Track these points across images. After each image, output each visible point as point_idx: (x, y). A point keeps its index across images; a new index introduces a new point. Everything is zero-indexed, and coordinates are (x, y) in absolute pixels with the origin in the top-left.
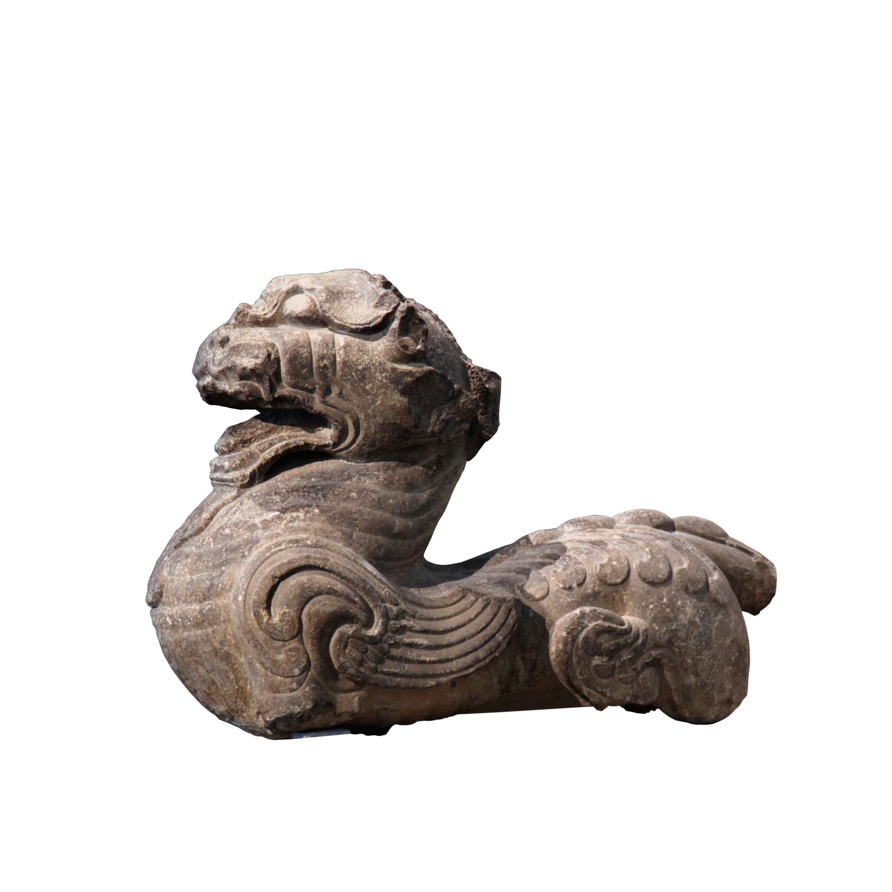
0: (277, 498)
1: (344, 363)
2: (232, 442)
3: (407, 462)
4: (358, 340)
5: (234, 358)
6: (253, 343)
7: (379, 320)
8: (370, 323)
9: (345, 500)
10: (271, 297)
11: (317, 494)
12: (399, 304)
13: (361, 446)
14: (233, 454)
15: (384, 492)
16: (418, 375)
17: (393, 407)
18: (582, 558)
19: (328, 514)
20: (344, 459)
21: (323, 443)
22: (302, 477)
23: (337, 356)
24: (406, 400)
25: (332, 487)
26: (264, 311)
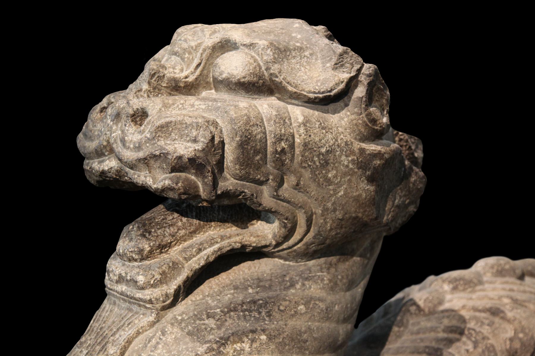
0: (211, 323)
1: (305, 145)
2: (147, 248)
3: (347, 254)
4: (316, 113)
5: (162, 143)
6: (188, 121)
7: (342, 86)
8: (330, 91)
9: (293, 316)
10: (190, 53)
11: (260, 313)
12: (363, 65)
13: (307, 245)
14: (147, 262)
15: (330, 298)
16: (386, 156)
17: (357, 199)
18: (486, 330)
19: (277, 340)
20: (280, 257)
21: (263, 243)
22: (236, 288)
23: (296, 136)
24: (372, 188)
25: (275, 300)
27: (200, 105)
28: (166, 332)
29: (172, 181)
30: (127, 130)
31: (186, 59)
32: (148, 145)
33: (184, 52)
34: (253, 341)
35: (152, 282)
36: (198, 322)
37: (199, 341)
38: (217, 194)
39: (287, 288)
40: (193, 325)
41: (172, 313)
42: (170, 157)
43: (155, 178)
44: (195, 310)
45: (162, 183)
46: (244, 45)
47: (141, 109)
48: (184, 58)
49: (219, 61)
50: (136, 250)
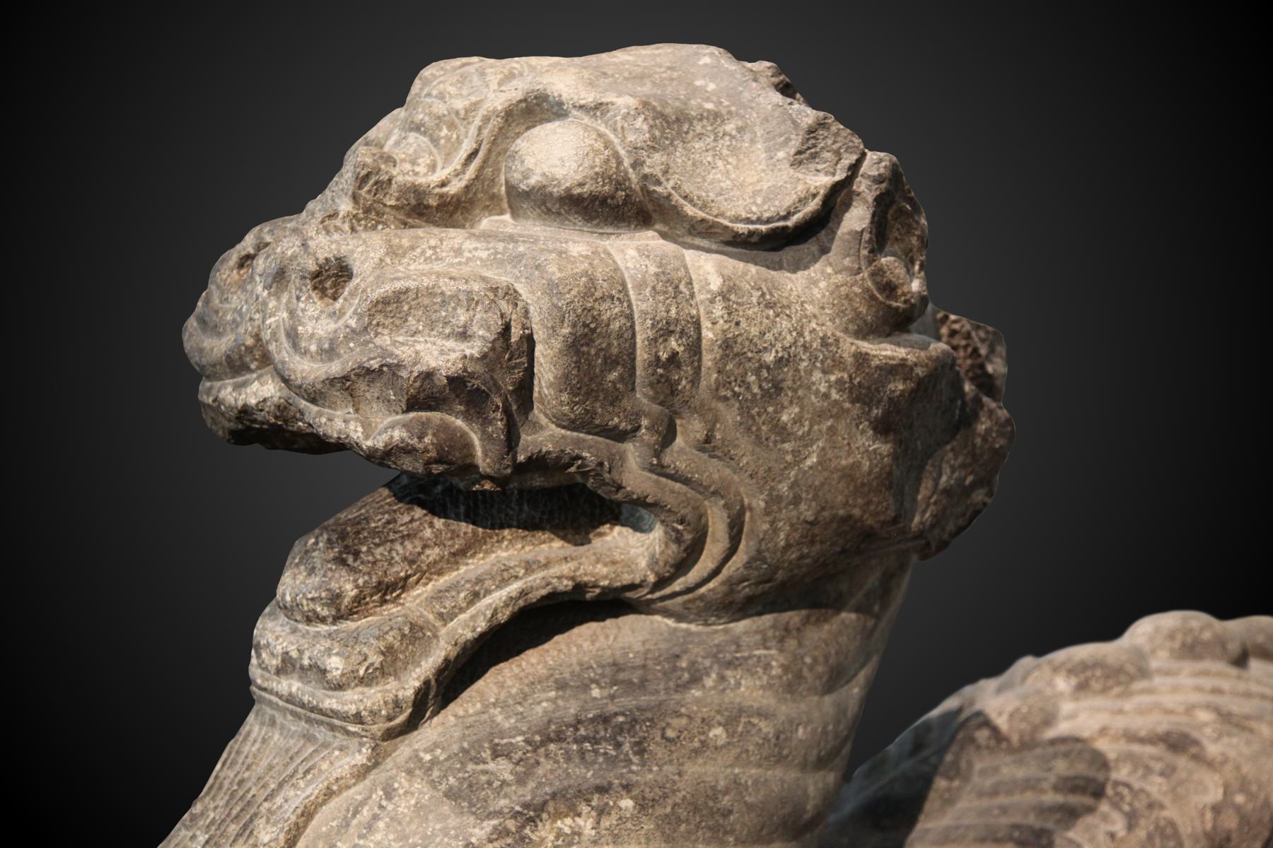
0: (503, 768)
1: (727, 345)
2: (350, 591)
3: (826, 606)
4: (753, 269)
5: (385, 340)
6: (448, 287)
7: (813, 205)
8: (785, 218)
9: (696, 752)
10: (452, 126)
11: (618, 745)
12: (863, 155)
13: (731, 583)
14: (349, 625)
15: (785, 710)
16: (919, 371)
17: (848, 474)
18: (1156, 786)
19: (660, 811)
20: (667, 613)
21: (627, 579)
22: (561, 686)
23: (705, 324)
24: (885, 448)
25: (655, 716)
27: (476, 249)
28: (395, 790)
29: (408, 431)
30: (303, 310)
31: (442, 142)
32: (352, 345)
33: (437, 125)
34: (602, 812)
35: (362, 672)
36: (470, 767)
37: (474, 813)
38: (511, 462)
39: (683, 687)
40: (460, 775)
41: (410, 745)
42: (404, 374)
43: (370, 424)
44: (463, 737)
45: (385, 437)
46: (581, 107)
47: (337, 259)
48: (439, 139)
50: (323, 595)
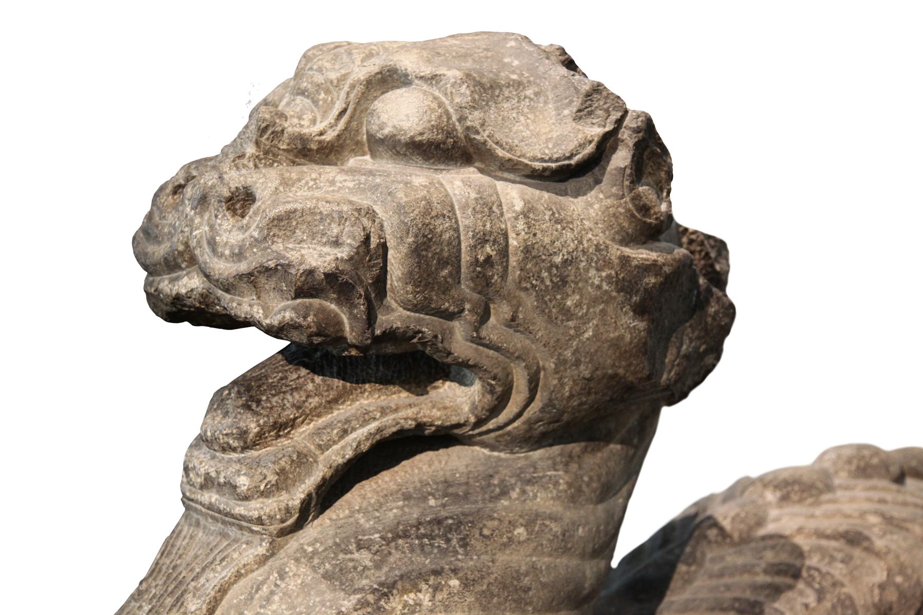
0: (365, 557)
1: (527, 250)
2: (254, 429)
3: (599, 440)
4: (546, 195)
5: (279, 246)
6: (325, 208)
7: (590, 149)
8: (569, 158)
9: (505, 545)
10: (327, 92)
11: (448, 541)
13: (530, 423)
14: (253, 453)
15: (569, 515)
16: (667, 269)
17: (615, 344)
18: (838, 570)
19: (478, 588)
20: (483, 445)
21: (454, 420)
22: (407, 497)
23: (511, 235)
24: (642, 325)
25: (475, 519)
26: (317, 124)
27: (345, 181)
28: (286, 573)
29: (296, 313)
30: (220, 225)
31: (321, 103)
32: (255, 250)
33: (317, 91)
34: (436, 589)
35: (262, 488)
36: (341, 556)
37: (344, 590)
39: (496, 498)
40: (334, 562)
41: (297, 540)
42: (293, 271)
43: (268, 308)
44: (336, 535)
45: (279, 317)
46: (421, 78)
47: (244, 188)
48: (318, 100)
49: (378, 105)
50: (235, 431)
